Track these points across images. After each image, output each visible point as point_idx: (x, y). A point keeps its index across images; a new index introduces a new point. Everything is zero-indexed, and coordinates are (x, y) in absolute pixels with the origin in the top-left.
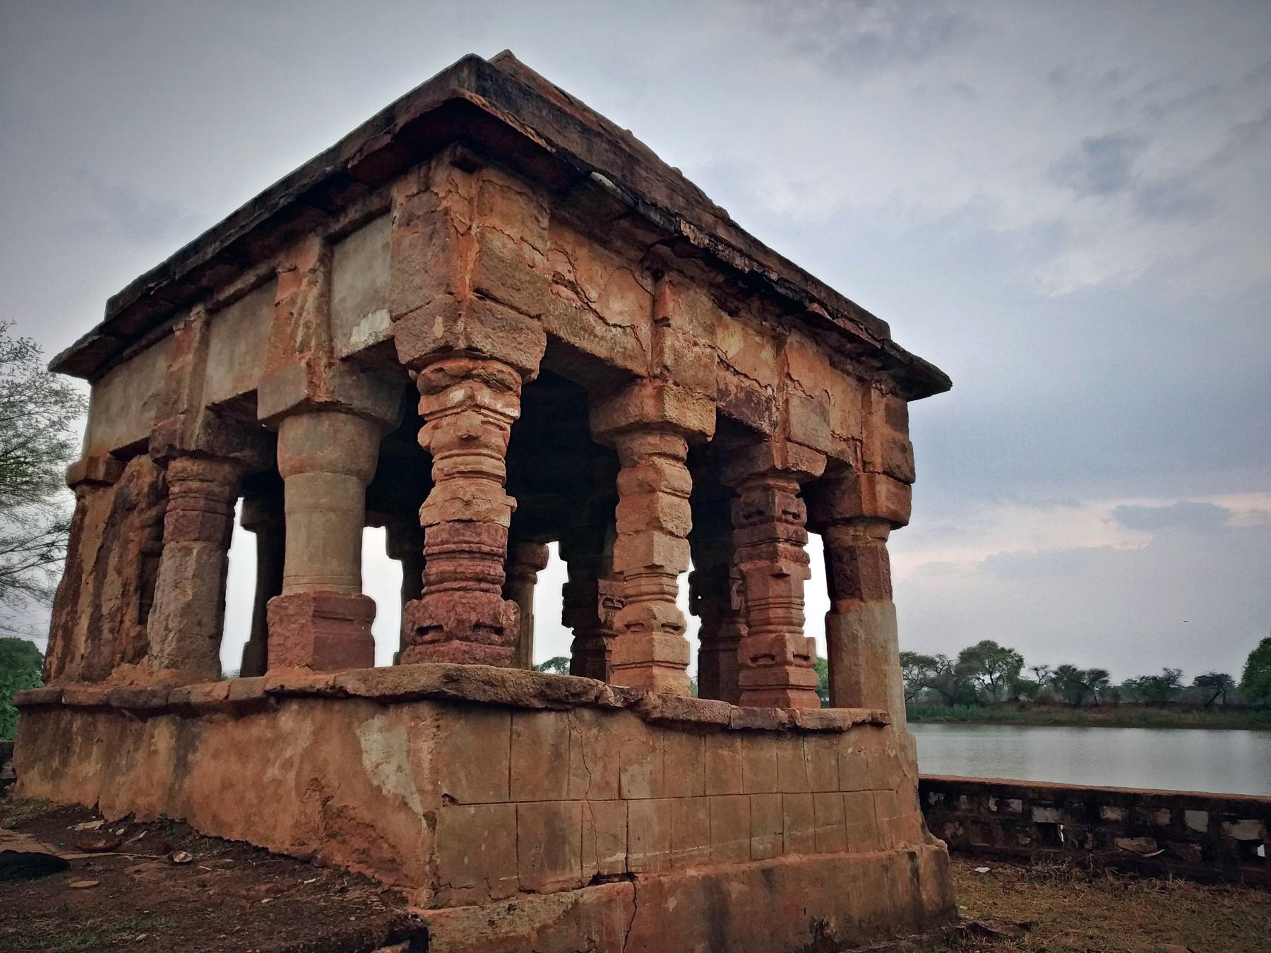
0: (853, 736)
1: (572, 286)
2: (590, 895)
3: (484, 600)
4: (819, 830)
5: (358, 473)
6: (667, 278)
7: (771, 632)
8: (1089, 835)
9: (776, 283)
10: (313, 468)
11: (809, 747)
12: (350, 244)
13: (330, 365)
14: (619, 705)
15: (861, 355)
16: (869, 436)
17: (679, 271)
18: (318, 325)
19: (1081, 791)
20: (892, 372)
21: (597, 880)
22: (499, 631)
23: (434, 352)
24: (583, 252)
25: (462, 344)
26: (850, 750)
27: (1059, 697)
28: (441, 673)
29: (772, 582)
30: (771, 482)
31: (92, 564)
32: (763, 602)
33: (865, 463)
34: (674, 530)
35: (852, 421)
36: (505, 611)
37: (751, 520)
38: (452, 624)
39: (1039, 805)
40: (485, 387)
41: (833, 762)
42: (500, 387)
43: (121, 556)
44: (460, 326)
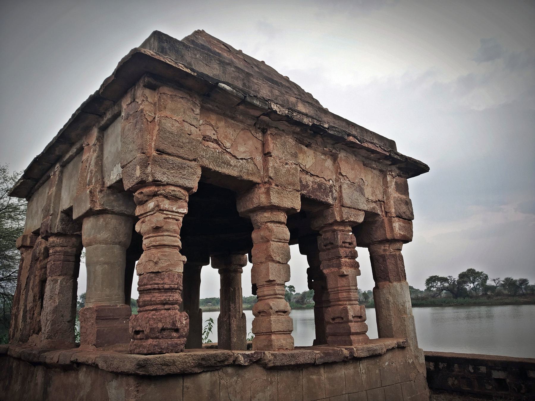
0: (388, 356)
1: (216, 141)
3: (167, 314)
5: (119, 243)
6: (269, 132)
7: (341, 305)
8: (522, 385)
9: (328, 129)
10: (96, 243)
11: (362, 366)
12: (110, 130)
13: (101, 191)
14: (246, 364)
15: (379, 159)
16: (388, 198)
17: (276, 128)
18: (96, 171)
19: (516, 363)
20: (397, 166)
22: (177, 330)
23: (137, 184)
24: (222, 124)
25: (150, 179)
26: (387, 363)
27: (506, 292)
28: (135, 363)
29: (339, 279)
30: (336, 228)
31: (24, 285)
32: (336, 289)
33: (386, 213)
34: (281, 261)
35: (378, 192)
36: (179, 319)
37: (327, 247)
38: (147, 331)
39: (495, 369)
40: (165, 200)
41: (377, 371)
42: (175, 198)
43: (33, 283)
44: (149, 168)
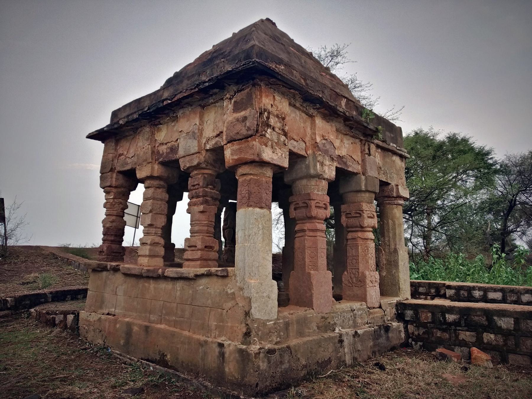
2: (103, 317)
4: (177, 319)
21: (108, 314)
